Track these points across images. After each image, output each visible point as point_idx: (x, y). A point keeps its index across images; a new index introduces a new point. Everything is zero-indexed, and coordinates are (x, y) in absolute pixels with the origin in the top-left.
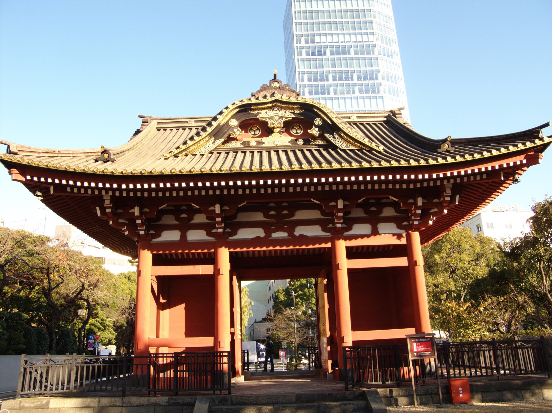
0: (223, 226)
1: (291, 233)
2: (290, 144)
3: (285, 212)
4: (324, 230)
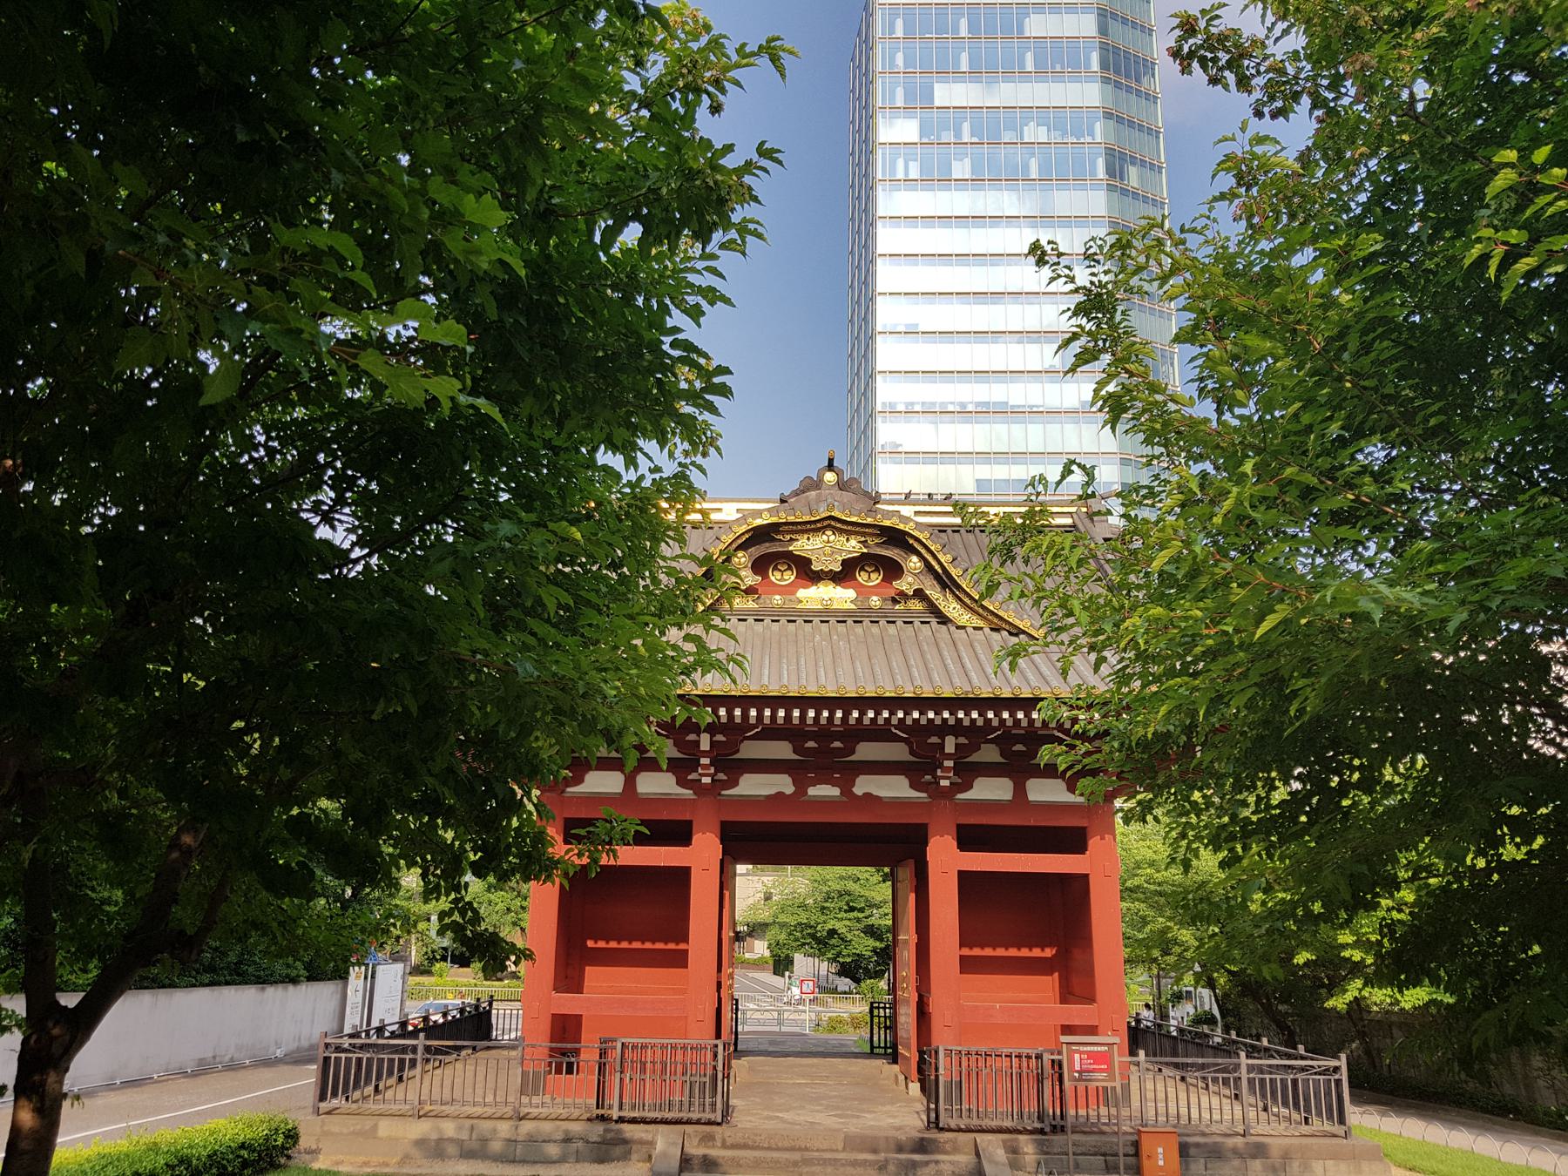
1: (847, 791)
3: (837, 744)
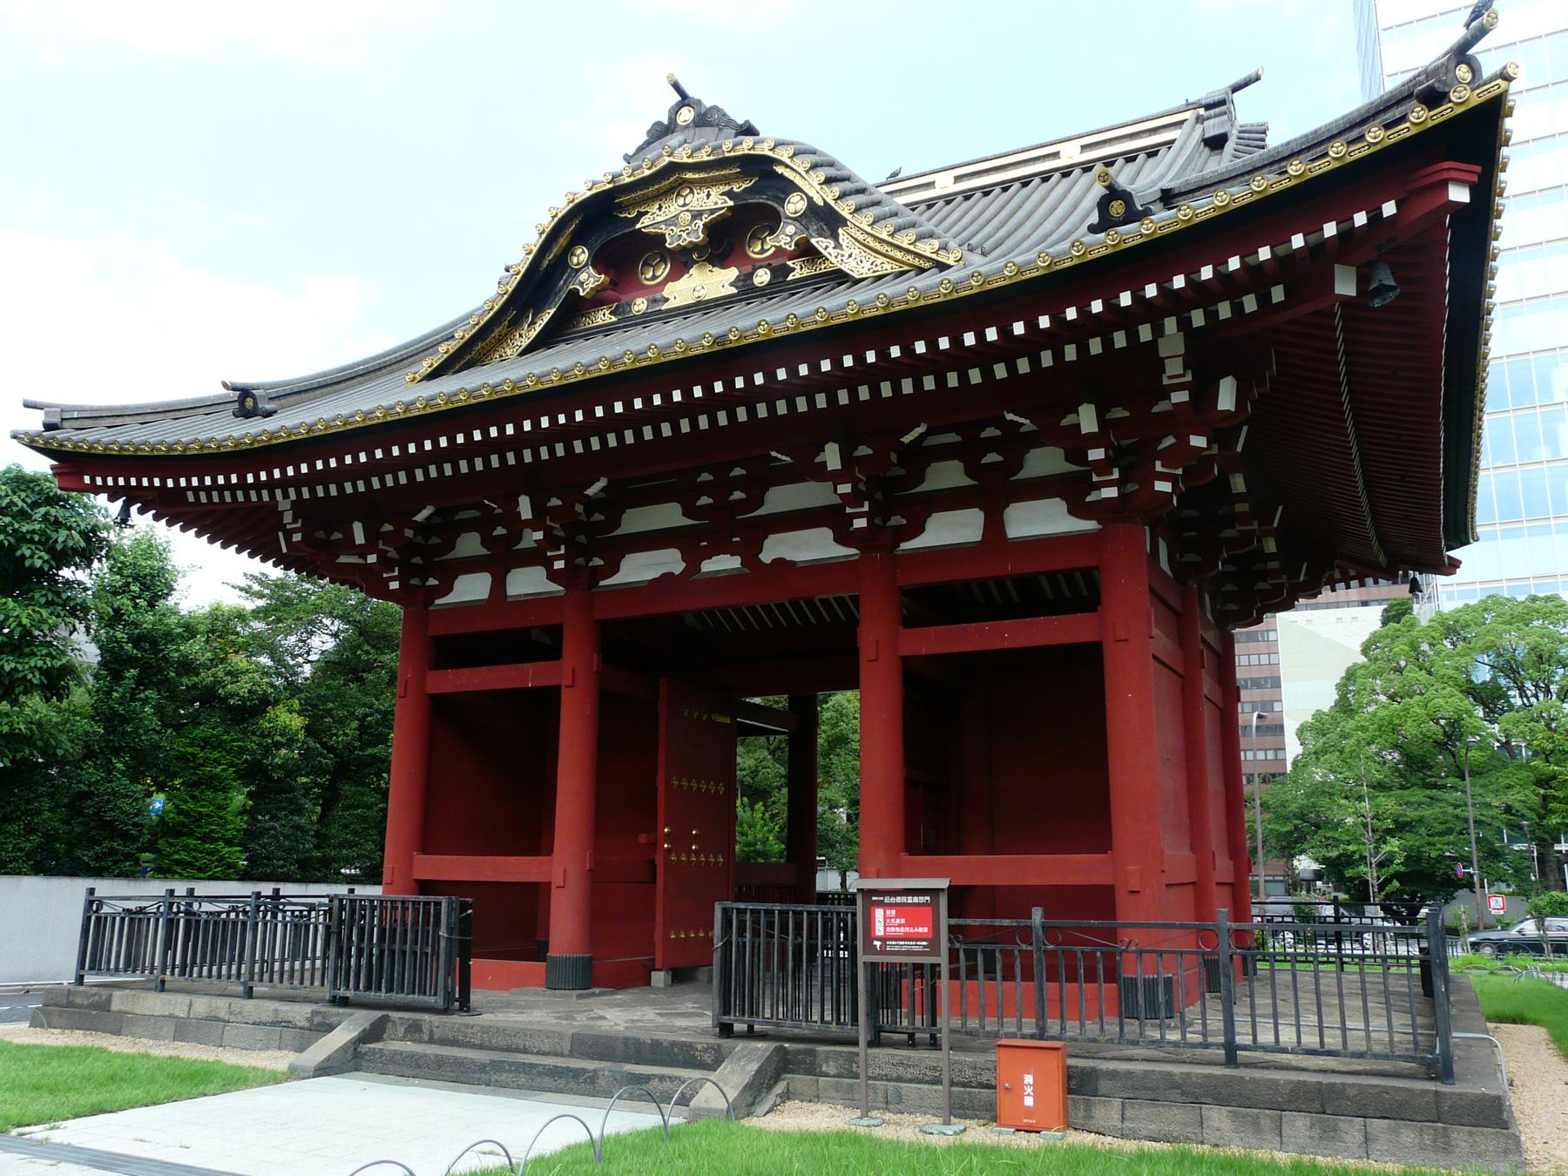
0: (1116, 475)
2: (735, 291)
3: (738, 495)
4: (1076, 510)
